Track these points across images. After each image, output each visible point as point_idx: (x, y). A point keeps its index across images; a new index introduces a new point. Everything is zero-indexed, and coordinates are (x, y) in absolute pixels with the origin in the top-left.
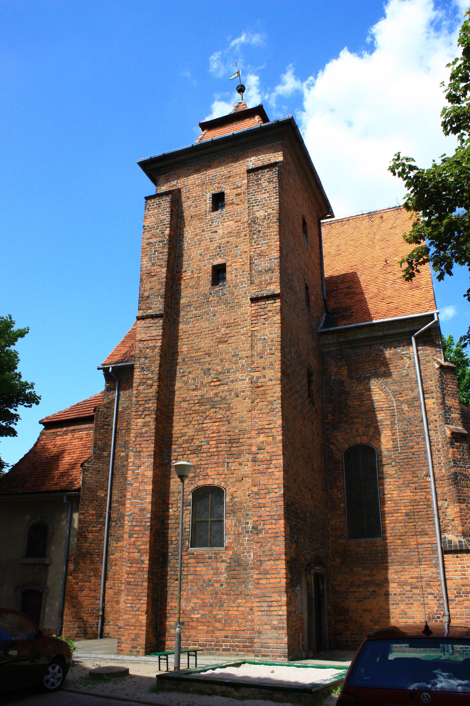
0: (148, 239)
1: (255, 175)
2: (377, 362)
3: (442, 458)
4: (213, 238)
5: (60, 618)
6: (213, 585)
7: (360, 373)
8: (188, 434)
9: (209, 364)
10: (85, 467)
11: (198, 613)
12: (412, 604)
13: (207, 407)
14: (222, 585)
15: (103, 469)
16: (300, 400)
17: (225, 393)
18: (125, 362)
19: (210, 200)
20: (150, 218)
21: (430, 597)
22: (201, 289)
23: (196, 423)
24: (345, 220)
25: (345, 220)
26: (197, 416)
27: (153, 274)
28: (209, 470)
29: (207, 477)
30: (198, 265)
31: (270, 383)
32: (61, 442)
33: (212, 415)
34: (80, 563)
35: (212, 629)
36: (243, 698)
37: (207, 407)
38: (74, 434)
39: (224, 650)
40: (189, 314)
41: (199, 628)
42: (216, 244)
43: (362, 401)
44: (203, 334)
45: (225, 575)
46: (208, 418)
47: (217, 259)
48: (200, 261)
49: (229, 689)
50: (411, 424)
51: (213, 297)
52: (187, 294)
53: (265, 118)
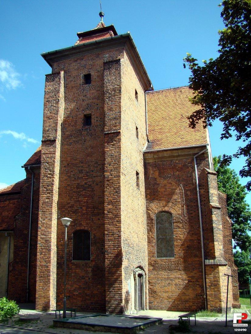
0: (47, 98)
1: (108, 65)
2: (175, 169)
3: (207, 219)
4: (84, 99)
5: (6, 293)
6: (85, 278)
7: (165, 175)
8: (71, 203)
9: (82, 167)
10: (16, 218)
11: (77, 292)
12: (189, 289)
13: (81, 189)
14: (89, 279)
15: (26, 219)
16: (132, 188)
17: (91, 183)
18: (37, 164)
19: (82, 78)
20: (48, 87)
21: (198, 286)
22: (78, 127)
23: (75, 197)
24: (161, 91)
25: (161, 91)
26: (76, 194)
27: (50, 118)
28: (82, 222)
29: (81, 225)
30: (76, 114)
31: (115, 179)
32: (3, 205)
33: (84, 194)
34: (15, 266)
35: (84, 299)
36: (95, 331)
37: (81, 189)
38: (10, 201)
39: (90, 309)
40: (71, 140)
41: (78, 299)
42: (86, 103)
43: (166, 189)
44: (79, 151)
45: (91, 274)
46: (82, 195)
47: (86, 111)
48: (77, 112)
49: (89, 327)
50: (191, 201)
51: (84, 131)
52: (70, 129)
53: (115, 33)
